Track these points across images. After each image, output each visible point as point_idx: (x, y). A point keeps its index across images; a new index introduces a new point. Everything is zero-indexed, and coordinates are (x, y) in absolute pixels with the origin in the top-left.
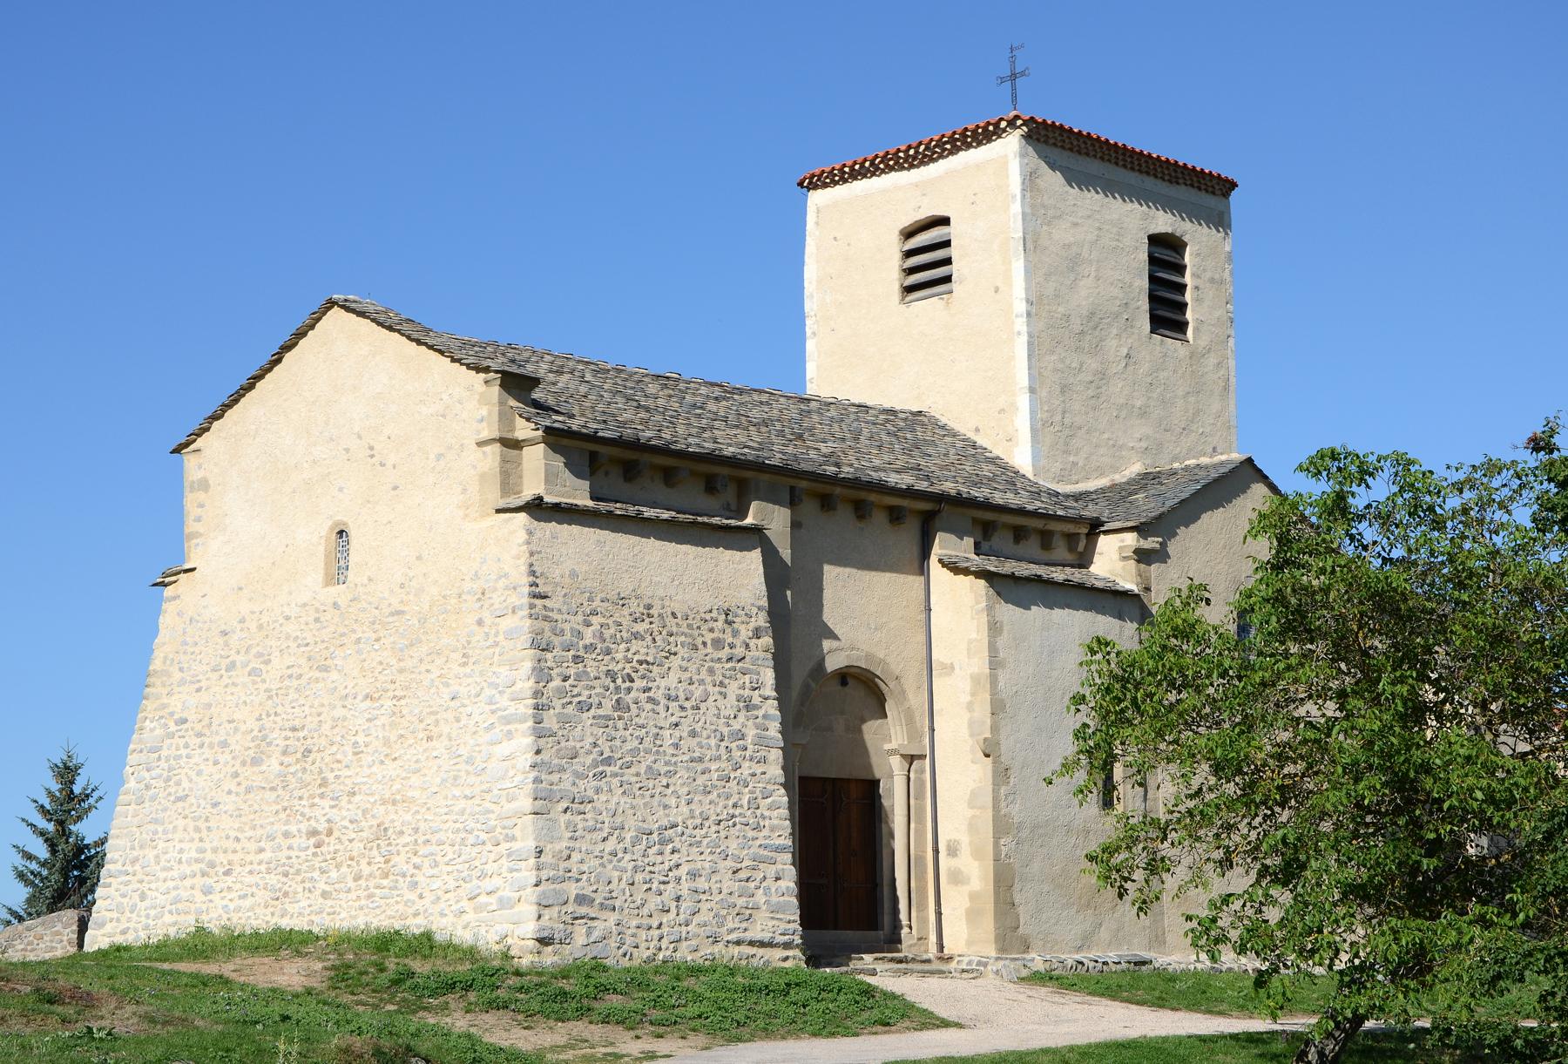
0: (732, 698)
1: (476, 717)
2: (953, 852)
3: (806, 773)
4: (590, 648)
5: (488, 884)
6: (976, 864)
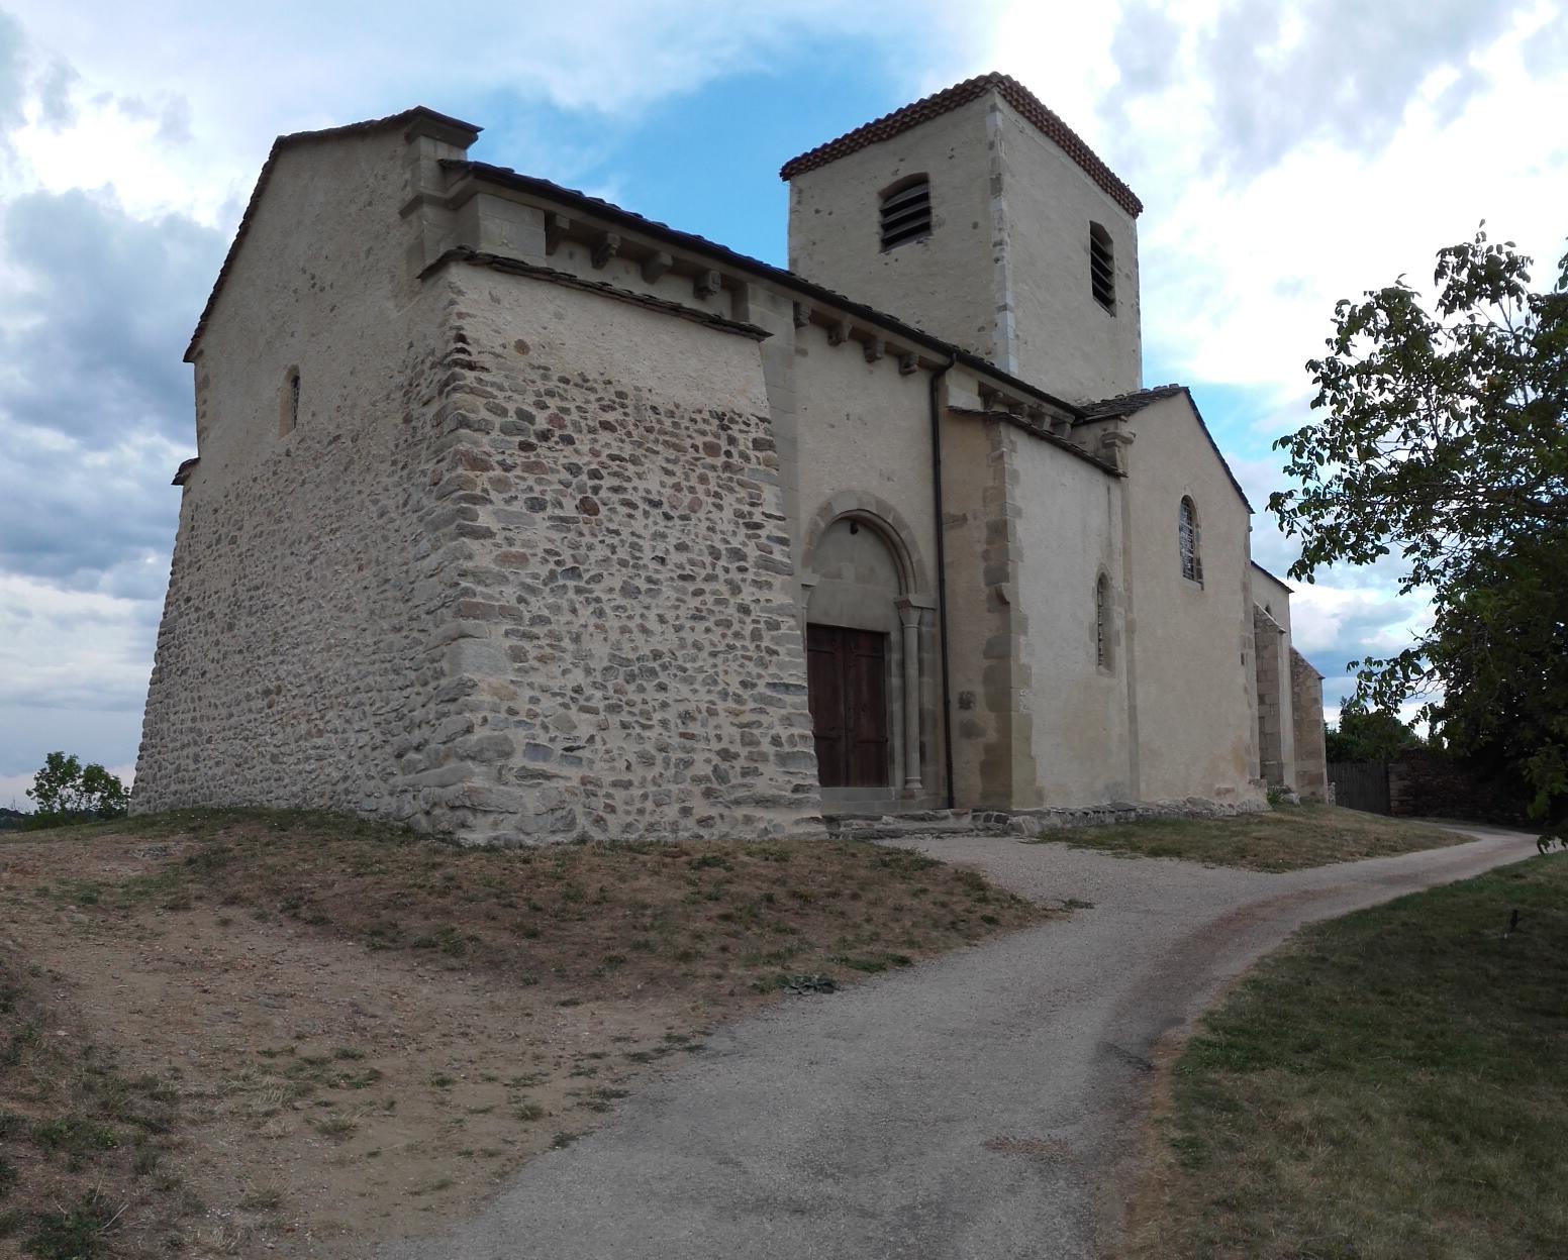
0: (728, 513)
1: (405, 531)
2: (966, 703)
3: (813, 621)
4: (544, 436)
5: (417, 736)
6: (993, 715)
